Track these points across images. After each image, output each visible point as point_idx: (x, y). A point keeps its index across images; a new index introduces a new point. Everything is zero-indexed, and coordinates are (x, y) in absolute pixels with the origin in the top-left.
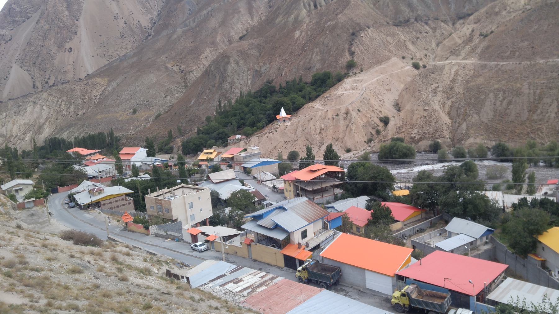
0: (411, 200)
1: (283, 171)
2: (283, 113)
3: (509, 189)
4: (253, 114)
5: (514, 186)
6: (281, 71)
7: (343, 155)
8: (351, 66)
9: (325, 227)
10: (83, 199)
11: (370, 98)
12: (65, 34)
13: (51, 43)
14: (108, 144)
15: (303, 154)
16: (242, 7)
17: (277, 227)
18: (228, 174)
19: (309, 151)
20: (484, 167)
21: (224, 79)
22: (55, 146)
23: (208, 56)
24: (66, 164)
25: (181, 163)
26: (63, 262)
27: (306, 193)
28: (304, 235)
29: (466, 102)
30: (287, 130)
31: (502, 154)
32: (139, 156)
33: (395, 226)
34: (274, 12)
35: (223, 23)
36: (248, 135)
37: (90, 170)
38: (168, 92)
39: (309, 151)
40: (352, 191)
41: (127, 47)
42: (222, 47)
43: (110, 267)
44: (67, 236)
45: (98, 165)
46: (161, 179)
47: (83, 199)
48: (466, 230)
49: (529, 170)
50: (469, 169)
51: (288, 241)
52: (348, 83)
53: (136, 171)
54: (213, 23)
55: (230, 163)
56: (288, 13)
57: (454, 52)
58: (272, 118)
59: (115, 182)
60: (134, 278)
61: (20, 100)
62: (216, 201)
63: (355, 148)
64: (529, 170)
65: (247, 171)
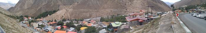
0: (66, 25)
1: (48, 22)
2: (49, 15)
3: (77, 24)
4: (45, 15)
5: (77, 24)
6: (48, 10)
7: (57, 21)
8: (58, 10)
9: (54, 30)
10: (24, 22)
11: (61, 14)
12: (24, 4)
13: (23, 5)
14: (27, 17)
15: (51, 20)
16: (44, 2)
17: (47, 29)
18: (41, 22)
19: (52, 20)
20: (74, 21)
21: (41, 10)
22: (22, 16)
23: (39, 7)
24: (23, 18)
25: (35, 20)
26: (21, 29)
27: (52, 25)
28: (51, 30)
29: (72, 14)
30: (49, 17)
31: (76, 20)
32: (30, 18)
33: (64, 29)
34: (48, 2)
35: (41, 4)
36: (44, 18)
37: (25, 19)
38: (34, 12)
39: (52, 20)
40: (58, 25)
41: (30, 6)
42: (41, 7)
43: (26, 30)
44: (22, 26)
45: (26, 19)
46: (32, 21)
47: (24, 22)
48: (72, 29)
49: (79, 22)
50: (72, 22)
51: (48, 31)
52: (58, 12)
53: (30, 20)
54: (40, 4)
55: (41, 21)
56: (50, 3)
57: (70, 9)
58: (47, 16)
59: (28, 21)
60: (28, 32)
61: (19, 11)
62: (39, 25)
63: (59, 20)
64: (79, 22)
65: (43, 22)
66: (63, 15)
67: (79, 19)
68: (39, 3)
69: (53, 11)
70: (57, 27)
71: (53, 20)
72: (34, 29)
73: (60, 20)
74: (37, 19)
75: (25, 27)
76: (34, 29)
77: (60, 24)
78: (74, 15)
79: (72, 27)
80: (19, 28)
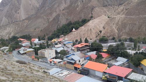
2: (74, 30)
3: (133, 49)
4: (66, 30)
6: (74, 19)
8: (92, 17)
9: (85, 59)
10: (22, 52)
13: (13, 11)
14: (28, 38)
15: (79, 40)
16: (63, 2)
17: (72, 59)
18: (59, 45)
19: (81, 39)
20: (126, 43)
21: (58, 21)
22: (14, 38)
23: (54, 15)
24: (17, 43)
25: (47, 43)
26: (16, 69)
27: (80, 50)
28: (79, 61)
29: (122, 26)
30: (75, 34)
31: (131, 40)
32: (36, 41)
33: (103, 59)
34: (71, 3)
35: (58, 6)
36: (65, 35)
37: (23, 45)
39: (81, 39)
40: (92, 50)
41: (33, 12)
42: (58, 12)
44: (18, 62)
45: (26, 43)
46: (42, 47)
47: (22, 52)
49: (138, 44)
50: (122, 44)
51: (75, 63)
52: (91, 22)
53: (35, 45)
54: (56, 6)
55: (60, 43)
57: (119, 14)
58: (71, 31)
59: (30, 48)
60: (35, 73)
62: (57, 53)
63: (93, 39)
64: (138, 44)
65: (64, 45)
66: (102, 29)
67: (139, 38)
68: (54, 5)
69: (81, 21)
70: (90, 54)
71: (82, 40)
72: (47, 63)
73: (95, 39)
74: (51, 39)
75: (25, 63)
76: (47, 63)
77: (96, 48)
78: (127, 27)
79: (121, 56)
80: (9, 68)
